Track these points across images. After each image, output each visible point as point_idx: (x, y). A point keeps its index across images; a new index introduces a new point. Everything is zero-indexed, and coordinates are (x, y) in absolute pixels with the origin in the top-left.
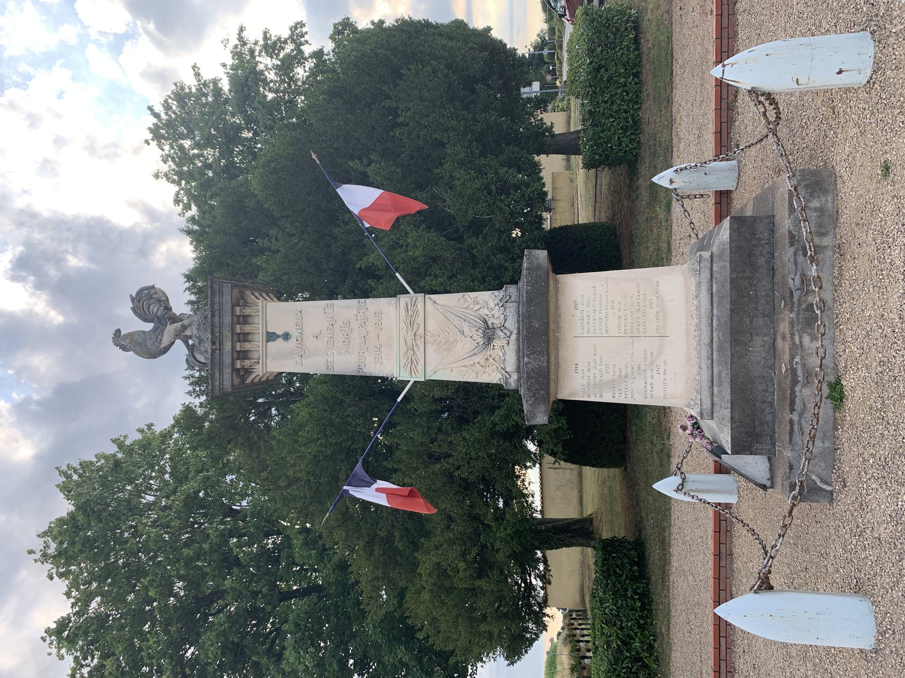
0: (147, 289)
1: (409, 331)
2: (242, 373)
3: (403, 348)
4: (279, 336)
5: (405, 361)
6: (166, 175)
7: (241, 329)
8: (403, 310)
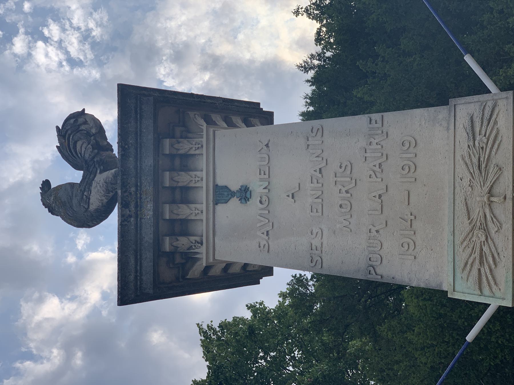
0: (74, 118)
1: (477, 189)
2: (178, 259)
3: (463, 225)
4: (232, 194)
5: (465, 255)
6: (307, 10)
7: (172, 179)
8: (462, 135)
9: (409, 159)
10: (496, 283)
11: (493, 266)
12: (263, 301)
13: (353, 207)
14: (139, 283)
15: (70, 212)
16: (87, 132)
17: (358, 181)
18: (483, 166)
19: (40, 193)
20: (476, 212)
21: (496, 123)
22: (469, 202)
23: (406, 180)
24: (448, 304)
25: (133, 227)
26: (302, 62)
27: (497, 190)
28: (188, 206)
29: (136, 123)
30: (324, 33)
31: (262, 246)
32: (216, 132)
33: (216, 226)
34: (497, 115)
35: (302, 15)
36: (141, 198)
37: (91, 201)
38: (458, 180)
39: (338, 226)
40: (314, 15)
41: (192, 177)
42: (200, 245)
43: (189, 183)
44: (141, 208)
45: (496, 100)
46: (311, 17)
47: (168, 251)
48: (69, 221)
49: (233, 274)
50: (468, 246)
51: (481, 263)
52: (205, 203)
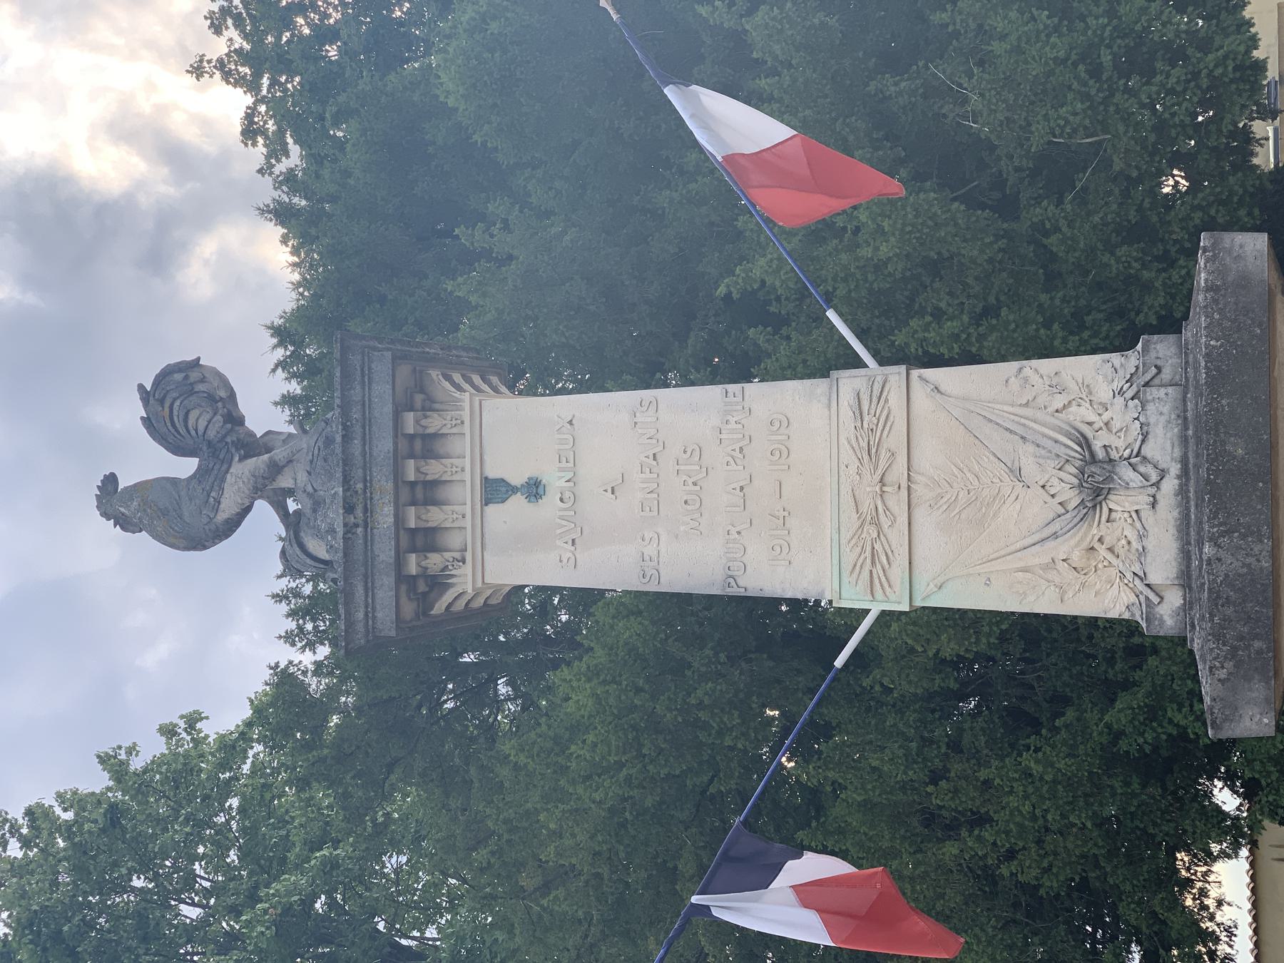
0: (180, 371)
2: (422, 587)
3: (850, 520)
4: (514, 490)
5: (854, 556)
6: (221, 65)
8: (847, 414)
9: (780, 442)
10: (890, 586)
11: (887, 566)
12: (135, 744)
13: (703, 503)
14: (370, 622)
15: (177, 525)
16: (209, 394)
17: (709, 470)
18: (874, 451)
19: (96, 495)
20: (866, 506)
21: (886, 401)
22: (856, 493)
23: (776, 468)
24: (647, 687)
25: (360, 541)
26: (268, 201)
27: (888, 479)
28: (441, 509)
29: (364, 389)
30: (263, 116)
31: (565, 561)
32: (483, 402)
33: (486, 536)
34: (888, 392)
35: (211, 76)
36: (371, 499)
37: (222, 506)
38: (843, 467)
39: (682, 528)
40: (239, 75)
41: (446, 467)
42: (461, 564)
43: (441, 476)
44: (371, 513)
45: (887, 375)
46: (232, 81)
47: (414, 574)
48: (172, 540)
49: (436, 616)
50: (856, 544)
51: (873, 562)
52: (469, 502)
